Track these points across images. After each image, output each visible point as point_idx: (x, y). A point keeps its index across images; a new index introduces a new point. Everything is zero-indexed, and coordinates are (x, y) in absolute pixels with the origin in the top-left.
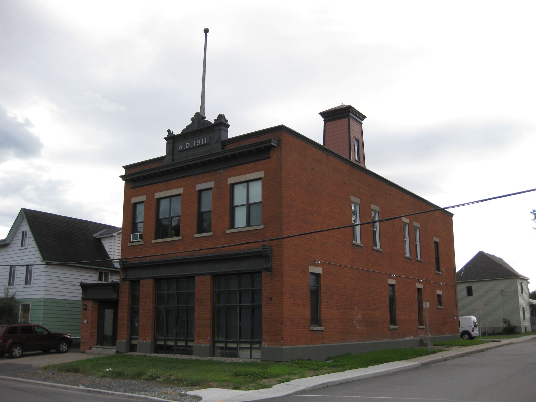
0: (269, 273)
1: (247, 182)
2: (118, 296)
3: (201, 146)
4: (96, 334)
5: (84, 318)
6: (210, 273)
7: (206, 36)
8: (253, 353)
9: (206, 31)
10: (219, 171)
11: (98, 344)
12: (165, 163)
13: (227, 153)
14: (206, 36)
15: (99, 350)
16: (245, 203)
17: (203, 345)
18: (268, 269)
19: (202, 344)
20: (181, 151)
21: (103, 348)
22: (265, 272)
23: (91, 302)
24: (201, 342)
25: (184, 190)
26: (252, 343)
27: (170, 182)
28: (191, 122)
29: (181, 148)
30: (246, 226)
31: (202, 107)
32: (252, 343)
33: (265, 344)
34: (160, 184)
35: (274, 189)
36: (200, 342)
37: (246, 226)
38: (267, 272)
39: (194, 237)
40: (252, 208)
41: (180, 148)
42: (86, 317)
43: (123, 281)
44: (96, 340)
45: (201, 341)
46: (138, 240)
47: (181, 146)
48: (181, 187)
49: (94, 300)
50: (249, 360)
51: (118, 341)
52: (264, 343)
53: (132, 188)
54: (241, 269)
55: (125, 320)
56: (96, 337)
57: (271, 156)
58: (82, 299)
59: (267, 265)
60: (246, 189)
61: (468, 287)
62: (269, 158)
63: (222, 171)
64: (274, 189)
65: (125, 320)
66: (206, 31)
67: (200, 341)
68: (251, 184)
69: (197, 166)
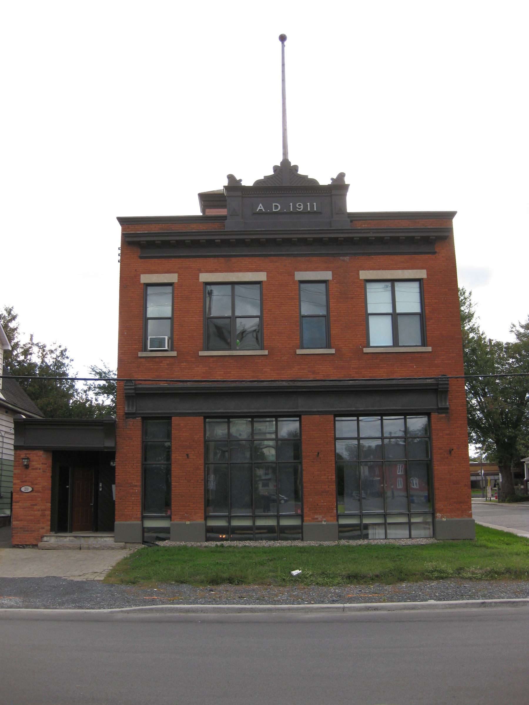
0: (444, 415)
1: (393, 281)
2: (116, 444)
3: (304, 213)
4: (49, 512)
5: (22, 482)
6: (202, 413)
7: (283, 46)
8: (388, 531)
9: (283, 38)
10: (341, 258)
11: (52, 530)
12: (195, 227)
13: (369, 232)
14: (283, 46)
15: (65, 540)
16: (390, 311)
17: (324, 523)
18: (445, 410)
19: (321, 521)
20: (261, 213)
21: (75, 537)
22: (436, 414)
23: (41, 453)
24: (320, 519)
25: (267, 276)
26: (409, 516)
27: (234, 260)
28: (273, 173)
29: (262, 208)
30: (392, 345)
31: (285, 153)
32: (409, 516)
33: (442, 516)
34: (212, 260)
35: (446, 299)
36: (317, 519)
37: (392, 345)
38: (439, 413)
39: (364, 352)
40: (400, 319)
41: (259, 208)
42: (26, 482)
43: (127, 418)
44: (49, 523)
45: (320, 517)
46: (166, 348)
47: (261, 205)
48: (261, 271)
49: (46, 450)
50: (383, 542)
51: (116, 523)
52: (440, 515)
53: (141, 258)
54: (395, 408)
55: (136, 486)
56: (49, 518)
57: (437, 250)
58: (15, 446)
59: (130, 409)
60: (390, 292)
61: (115, 454)
62: (434, 253)
63: (347, 258)
64: (446, 299)
65: (136, 486)
66: (283, 38)
67: (316, 517)
68: (398, 286)
69: (304, 242)
